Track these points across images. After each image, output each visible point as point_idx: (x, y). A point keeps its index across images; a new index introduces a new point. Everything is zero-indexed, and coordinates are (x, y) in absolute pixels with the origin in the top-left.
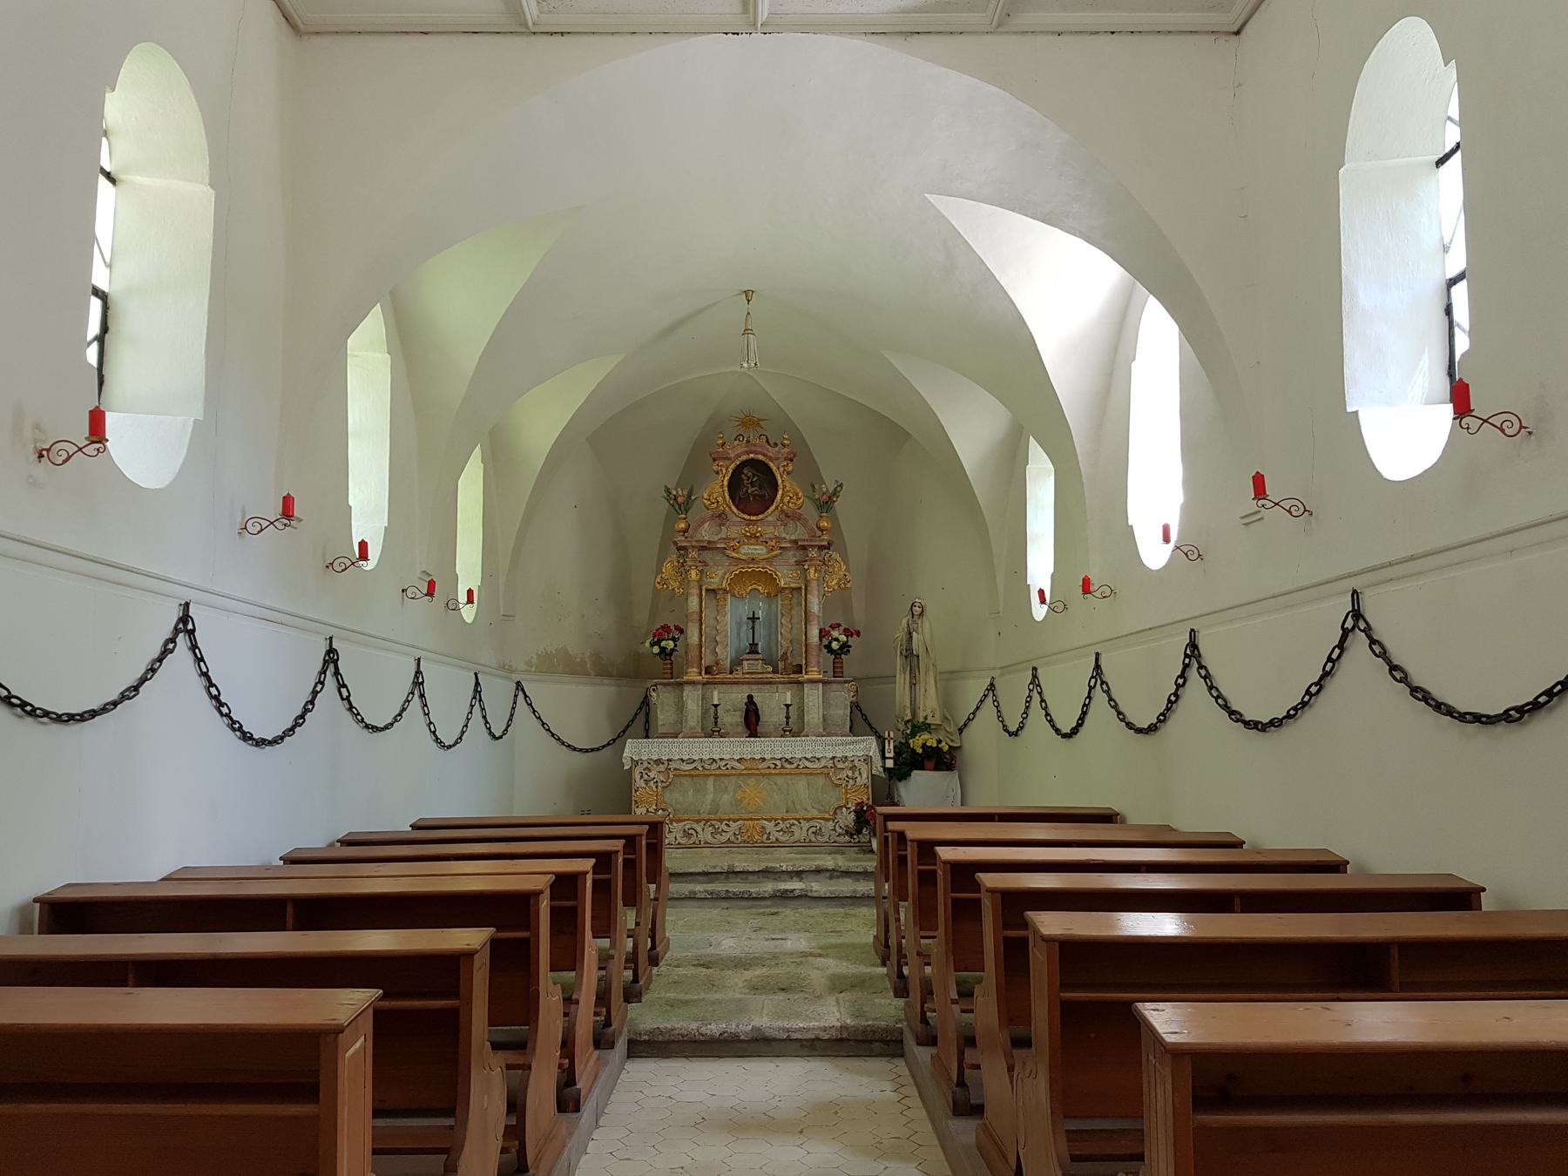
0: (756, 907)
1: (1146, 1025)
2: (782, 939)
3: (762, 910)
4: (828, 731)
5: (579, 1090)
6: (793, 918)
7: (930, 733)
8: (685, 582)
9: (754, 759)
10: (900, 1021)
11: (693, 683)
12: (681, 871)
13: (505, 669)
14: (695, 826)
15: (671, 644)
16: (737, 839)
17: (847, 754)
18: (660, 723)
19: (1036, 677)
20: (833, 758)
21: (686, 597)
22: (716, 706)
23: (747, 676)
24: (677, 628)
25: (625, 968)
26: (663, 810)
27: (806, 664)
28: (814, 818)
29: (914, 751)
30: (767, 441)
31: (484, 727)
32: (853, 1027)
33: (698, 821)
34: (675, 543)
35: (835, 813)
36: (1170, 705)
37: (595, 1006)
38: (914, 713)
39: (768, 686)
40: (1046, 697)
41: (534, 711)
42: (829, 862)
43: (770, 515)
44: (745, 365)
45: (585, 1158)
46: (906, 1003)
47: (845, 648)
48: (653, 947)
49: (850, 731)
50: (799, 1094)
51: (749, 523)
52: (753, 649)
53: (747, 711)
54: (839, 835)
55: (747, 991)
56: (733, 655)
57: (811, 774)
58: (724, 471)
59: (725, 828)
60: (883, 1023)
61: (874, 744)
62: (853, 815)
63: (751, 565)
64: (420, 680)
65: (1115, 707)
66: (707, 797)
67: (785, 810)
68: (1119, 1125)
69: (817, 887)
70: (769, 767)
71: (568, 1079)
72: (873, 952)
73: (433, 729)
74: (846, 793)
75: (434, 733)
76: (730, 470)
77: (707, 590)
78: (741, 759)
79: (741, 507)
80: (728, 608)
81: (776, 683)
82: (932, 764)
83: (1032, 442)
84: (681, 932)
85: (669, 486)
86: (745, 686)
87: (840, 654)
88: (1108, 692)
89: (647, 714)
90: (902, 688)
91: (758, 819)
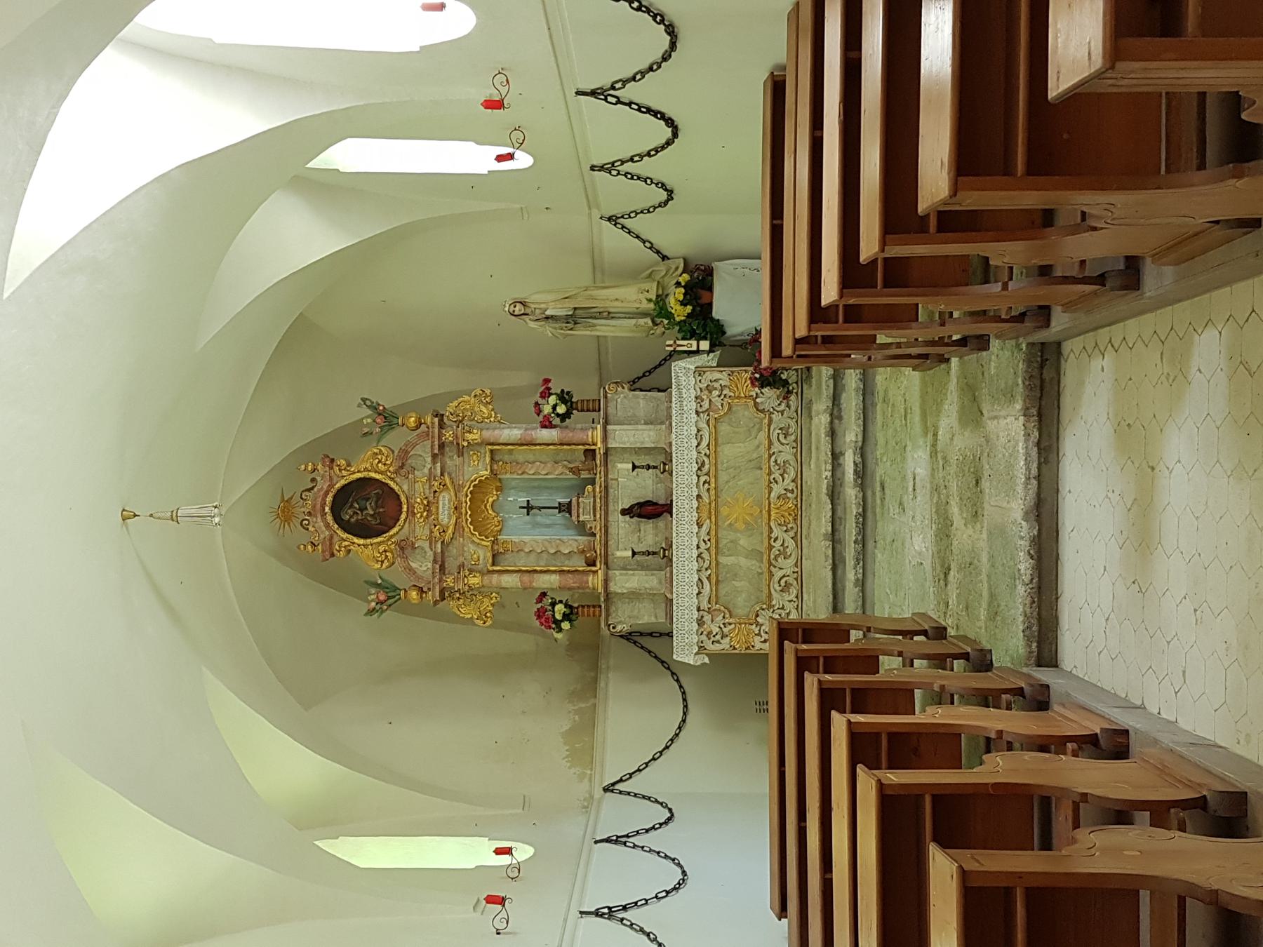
0: (874, 507)
1: (1078, 87)
2: (914, 479)
3: (878, 501)
4: (664, 419)
5: (1102, 729)
6: (889, 463)
7: (667, 295)
8: (482, 591)
9: (698, 508)
10: (1018, 346)
11: (606, 582)
12: (831, 596)
13: (588, 805)
14: (776, 578)
15: (560, 608)
16: (792, 528)
17: (693, 396)
18: (653, 620)
19: (602, 167)
20: (697, 413)
21: (501, 590)
22: (634, 553)
23: (598, 516)
24: (540, 600)
25: (952, 670)
26: (757, 616)
27: (583, 445)
28: (769, 436)
29: (689, 316)
30: (309, 490)
31: (659, 831)
32: (1025, 401)
33: (771, 575)
34: (436, 603)
35: (762, 411)
36: (643, 9)
37: (1000, 708)
38: (644, 314)
39: (611, 491)
40: (627, 155)
41: (639, 770)
42: (821, 421)
43: (400, 487)
44: (217, 520)
45: (1182, 724)
46: (997, 337)
47: (564, 397)
48: (924, 633)
49: (664, 391)
50: (1105, 469)
51: (411, 512)
52: (565, 508)
53: (640, 516)
54: (788, 406)
55: (978, 525)
56: (572, 532)
57: (716, 440)
58: (347, 543)
59: (779, 542)
60: (1021, 365)
61: (682, 363)
62: (766, 390)
63: (463, 510)
64: (606, 910)
65: (643, 73)
66: (742, 564)
67: (759, 471)
68: (1164, 101)
69: (851, 435)
70: (708, 490)
71: (1090, 745)
72: (932, 372)
73: (664, 894)
74: (739, 397)
75: (668, 892)
76: (345, 536)
77: (493, 564)
78: (698, 524)
79: (391, 523)
80: (515, 538)
81: (606, 481)
82: (704, 294)
83: (316, 163)
84: (905, 598)
85: (365, 611)
86: (610, 519)
87: (572, 403)
88: (625, 82)
89: (641, 634)
90: (613, 329)
91: (770, 504)
